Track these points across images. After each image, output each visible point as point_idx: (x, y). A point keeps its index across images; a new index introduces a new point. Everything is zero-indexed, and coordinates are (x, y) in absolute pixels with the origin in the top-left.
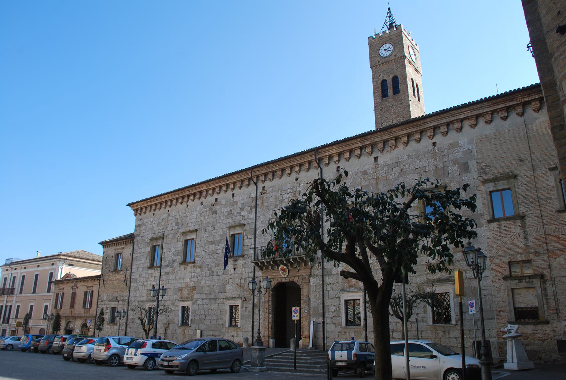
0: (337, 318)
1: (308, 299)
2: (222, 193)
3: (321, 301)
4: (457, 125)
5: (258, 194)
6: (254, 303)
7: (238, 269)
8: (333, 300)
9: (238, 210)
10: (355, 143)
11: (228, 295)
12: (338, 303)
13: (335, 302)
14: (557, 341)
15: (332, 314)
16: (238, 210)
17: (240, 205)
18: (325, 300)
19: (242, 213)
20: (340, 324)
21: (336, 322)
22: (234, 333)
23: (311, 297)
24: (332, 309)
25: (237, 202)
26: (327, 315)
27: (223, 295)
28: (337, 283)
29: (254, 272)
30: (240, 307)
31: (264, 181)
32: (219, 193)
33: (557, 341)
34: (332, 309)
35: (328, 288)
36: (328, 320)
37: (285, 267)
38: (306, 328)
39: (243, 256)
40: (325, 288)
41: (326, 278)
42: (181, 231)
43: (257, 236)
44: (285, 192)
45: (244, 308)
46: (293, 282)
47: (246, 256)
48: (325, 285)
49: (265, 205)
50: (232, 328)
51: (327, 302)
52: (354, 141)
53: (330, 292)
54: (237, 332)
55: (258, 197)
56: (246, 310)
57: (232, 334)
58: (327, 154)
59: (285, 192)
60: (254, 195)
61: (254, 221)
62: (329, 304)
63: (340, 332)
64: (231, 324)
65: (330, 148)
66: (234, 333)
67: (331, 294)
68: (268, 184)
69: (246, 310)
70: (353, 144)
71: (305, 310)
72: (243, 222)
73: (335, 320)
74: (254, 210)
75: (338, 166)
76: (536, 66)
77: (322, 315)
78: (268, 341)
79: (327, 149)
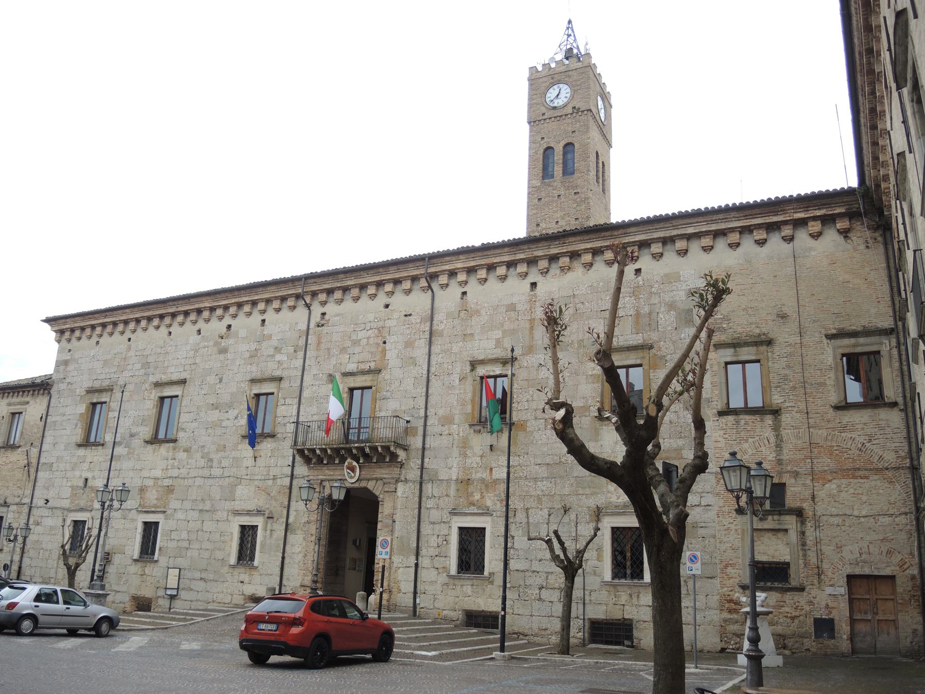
0: (443, 559)
1: (391, 522)
8: (437, 526)
11: (238, 505)
23: (397, 517)
41: (428, 488)
42: (153, 379)
45: (268, 532)
51: (426, 529)
57: (241, 579)
62: (430, 532)
69: (271, 535)
73: (439, 562)
75: (464, 290)
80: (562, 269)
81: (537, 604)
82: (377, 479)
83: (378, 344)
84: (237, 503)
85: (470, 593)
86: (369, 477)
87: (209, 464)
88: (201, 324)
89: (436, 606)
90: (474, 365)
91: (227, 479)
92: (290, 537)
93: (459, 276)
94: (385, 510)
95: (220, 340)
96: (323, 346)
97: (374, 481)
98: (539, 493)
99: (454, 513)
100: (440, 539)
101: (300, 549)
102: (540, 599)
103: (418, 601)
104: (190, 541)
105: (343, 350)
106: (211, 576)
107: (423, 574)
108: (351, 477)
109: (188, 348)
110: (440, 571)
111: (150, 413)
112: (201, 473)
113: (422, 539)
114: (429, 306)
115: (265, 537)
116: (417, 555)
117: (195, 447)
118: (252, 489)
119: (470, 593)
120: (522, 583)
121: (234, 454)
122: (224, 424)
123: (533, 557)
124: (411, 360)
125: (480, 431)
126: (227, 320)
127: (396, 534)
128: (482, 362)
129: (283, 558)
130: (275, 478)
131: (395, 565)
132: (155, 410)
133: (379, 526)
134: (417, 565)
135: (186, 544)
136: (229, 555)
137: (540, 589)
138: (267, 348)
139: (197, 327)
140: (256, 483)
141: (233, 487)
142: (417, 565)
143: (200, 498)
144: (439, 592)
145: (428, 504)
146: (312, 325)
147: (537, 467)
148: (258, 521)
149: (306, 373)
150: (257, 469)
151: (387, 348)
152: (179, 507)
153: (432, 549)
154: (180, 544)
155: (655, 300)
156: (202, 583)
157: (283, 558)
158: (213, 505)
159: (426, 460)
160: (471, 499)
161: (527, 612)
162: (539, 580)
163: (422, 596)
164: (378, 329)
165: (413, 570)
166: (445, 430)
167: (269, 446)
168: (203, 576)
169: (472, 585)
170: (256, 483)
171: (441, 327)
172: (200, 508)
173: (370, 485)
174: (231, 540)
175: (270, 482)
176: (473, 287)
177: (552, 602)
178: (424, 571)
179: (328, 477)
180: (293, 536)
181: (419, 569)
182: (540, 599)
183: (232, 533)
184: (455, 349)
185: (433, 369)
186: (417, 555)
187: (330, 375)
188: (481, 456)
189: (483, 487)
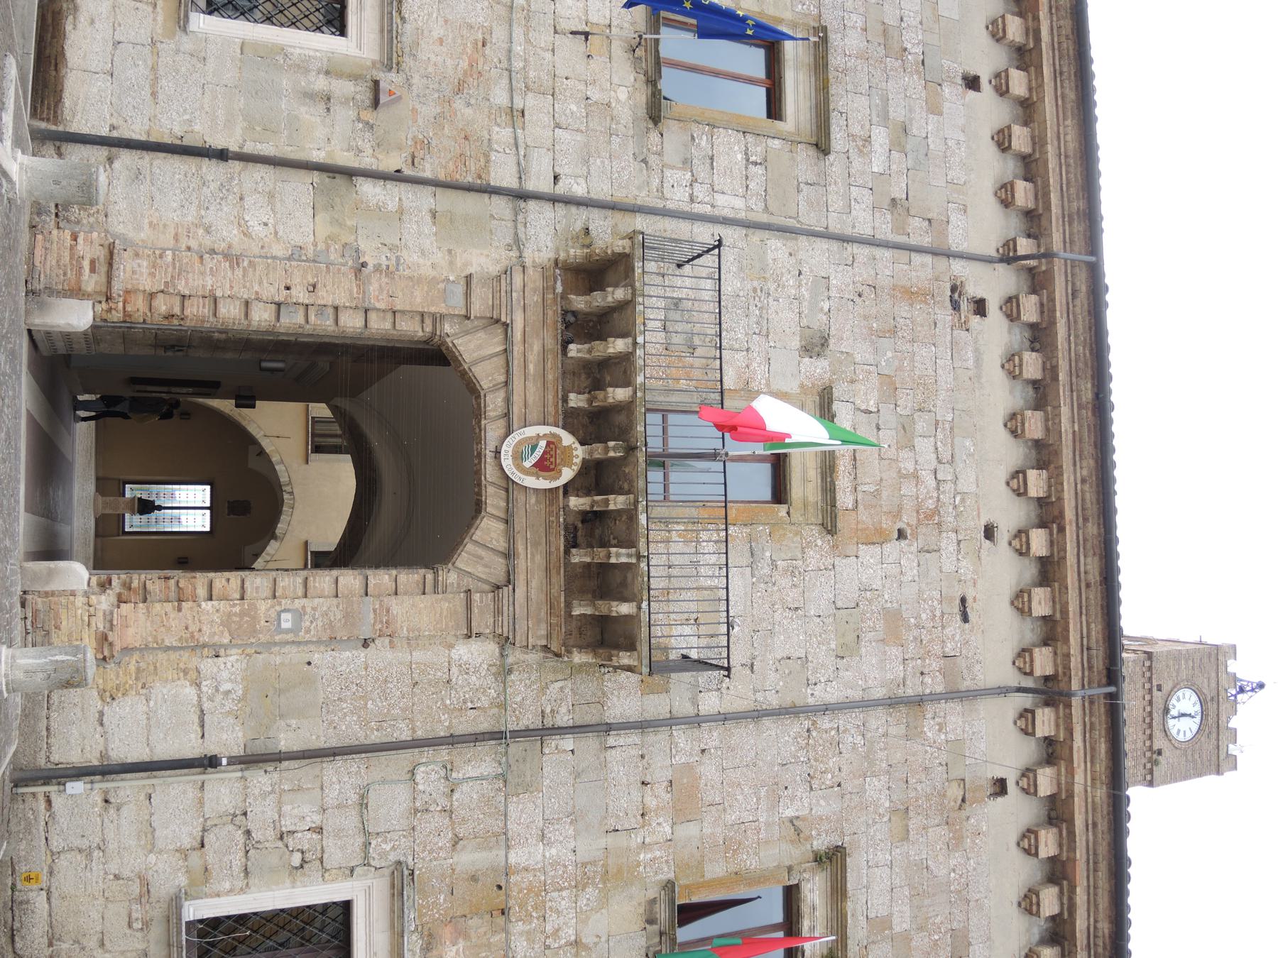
0: (237, 860)
3: (351, 730)
5: (958, 267)
6: (350, 174)
8: (350, 821)
9: (897, 113)
10: (1092, 903)
12: (335, 856)
13: (338, 833)
15: (262, 815)
16: (897, 113)
17: (922, 125)
18: (354, 764)
19: (880, 137)
20: (202, 879)
21: (210, 855)
23: (381, 654)
25: (934, 108)
26: (260, 779)
28: (456, 840)
29: (554, 200)
30: (325, 42)
31: (1011, 307)
34: (299, 814)
35: (429, 778)
36: (223, 790)
37: (567, 474)
39: (655, 112)
40: (428, 753)
41: (479, 765)
43: (756, 236)
44: (946, 456)
45: (321, 83)
46: (478, 508)
47: (654, 137)
48: (444, 753)
49: (903, 310)
51: (340, 779)
52: (1104, 901)
53: (401, 793)
55: (942, 263)
58: (1078, 742)
59: (946, 456)
60: (957, 239)
61: (835, 227)
62: (332, 795)
65: (1102, 766)
67: (391, 804)
68: (995, 334)
70: (1092, 891)
71: (299, 615)
72: (838, 139)
73: (225, 841)
74: (884, 228)
76: (786, 405)
77: (259, 748)
79: (1103, 747)
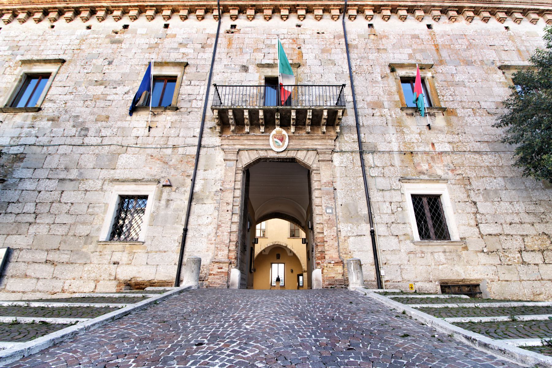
0: (401, 226)
1: (332, 189)
2: (142, 20)
4: (534, 16)
7: (160, 129)
8: (387, 194)
11: (118, 174)
14: (401, 77)
22: (123, 257)
23: (337, 185)
24: (386, 208)
27: (104, 174)
32: (135, 18)
33: (401, 77)
36: (380, 230)
38: (330, 242)
41: (369, 158)
42: (19, 58)
45: (163, 202)
48: (367, 168)
50: (116, 245)
51: (375, 196)
54: (131, 253)
56: (167, 205)
57: (115, 259)
62: (380, 199)
63: (411, 252)
64: (117, 231)
66: (123, 257)
67: (381, 183)
69: (167, 205)
73: (397, 229)
75: (166, 23)
78: (228, 274)
80: (198, 17)
81: (521, 268)
82: (308, 150)
83: (294, 49)
84: (118, 171)
85: (444, 261)
86: (298, 147)
87: (83, 133)
88: (93, 22)
89: (406, 277)
90: (393, 68)
91: (107, 148)
92: (195, 207)
93: (181, 11)
94: (319, 180)
95: (114, 34)
96: (234, 46)
97: (305, 152)
98: (488, 164)
99: (403, 179)
100: (394, 206)
101: (210, 220)
102: (524, 263)
103: (382, 272)
104: (36, 215)
105: (257, 50)
106: (65, 257)
107: (380, 242)
108: (279, 146)
109: (73, 37)
110: (401, 238)
111: (9, 86)
112: (69, 141)
113: (374, 207)
114: (216, 32)
115: (158, 208)
116: (371, 221)
117: (64, 117)
118: (144, 157)
119: (444, 261)
120: (499, 247)
121: (119, 124)
122: (109, 98)
123: (503, 221)
124: (330, 62)
125: (412, 115)
126: (126, 20)
127: (339, 202)
128: (402, 66)
129: (186, 230)
130: (174, 147)
131: (343, 234)
132: (16, 83)
133: (315, 194)
134: (372, 233)
135: (31, 219)
136: (99, 229)
137: (520, 252)
138: (168, 43)
139: (88, 23)
140: (149, 151)
141: (114, 156)
142: (372, 233)
143: (63, 166)
144: (406, 262)
145: (371, 172)
146: (222, 31)
147: (478, 144)
148: (150, 190)
149: (215, 63)
150: (150, 139)
151: (303, 52)
152: (29, 175)
153: (387, 216)
154: (19, 218)
155: (310, 50)
156: (48, 268)
157: (186, 230)
158: (81, 174)
159: (362, 135)
160: (419, 169)
161: (515, 277)
162: (517, 243)
163: (385, 266)
164: (293, 39)
165: (368, 239)
166: (377, 112)
167: (169, 118)
168: (51, 257)
169: (444, 252)
170: (149, 151)
171: (354, 43)
172: (61, 177)
173: (300, 156)
174: (105, 212)
175: (169, 151)
176: (377, 21)
177: (537, 265)
178: (382, 239)
179: (246, 147)
180: (200, 206)
181: (377, 238)
182: (524, 263)
183: (106, 205)
184: (371, 57)
185: (354, 69)
186: (371, 221)
187: (244, 66)
188: (420, 134)
189: (429, 159)
